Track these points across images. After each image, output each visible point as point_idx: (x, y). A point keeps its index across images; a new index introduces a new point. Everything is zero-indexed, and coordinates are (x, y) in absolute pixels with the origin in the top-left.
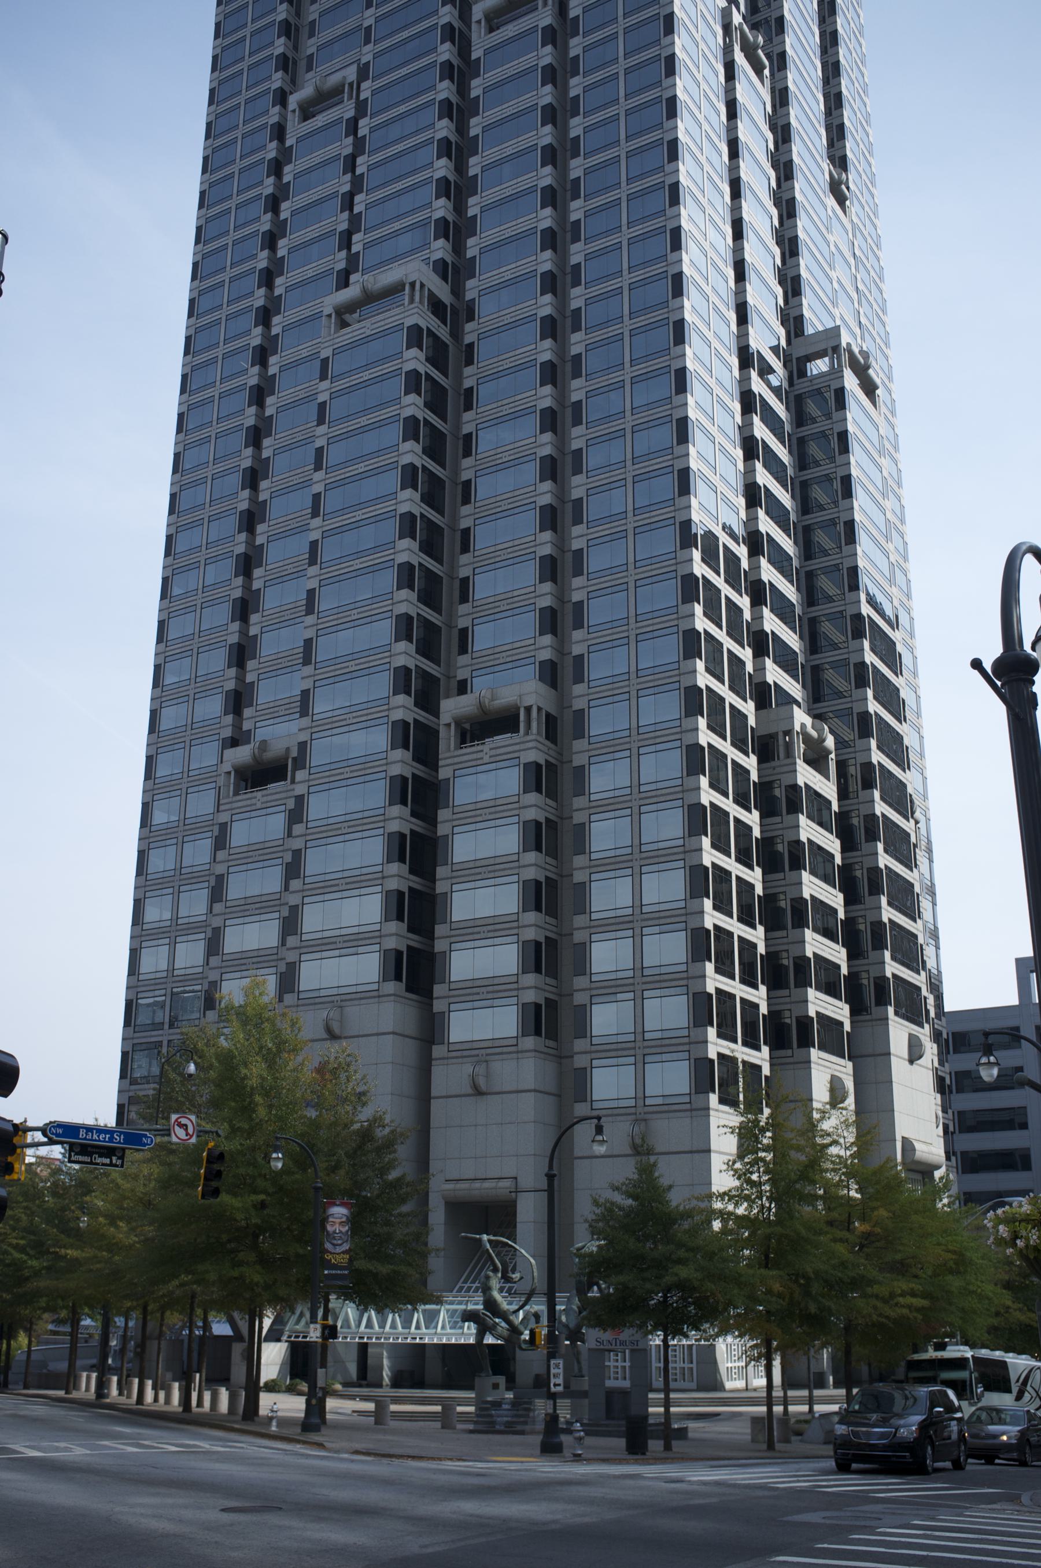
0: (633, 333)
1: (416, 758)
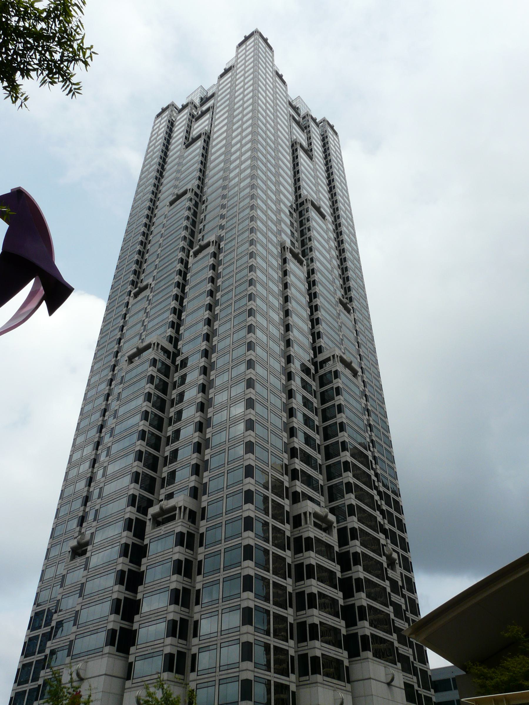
0: (222, 682)
1: (138, 511)
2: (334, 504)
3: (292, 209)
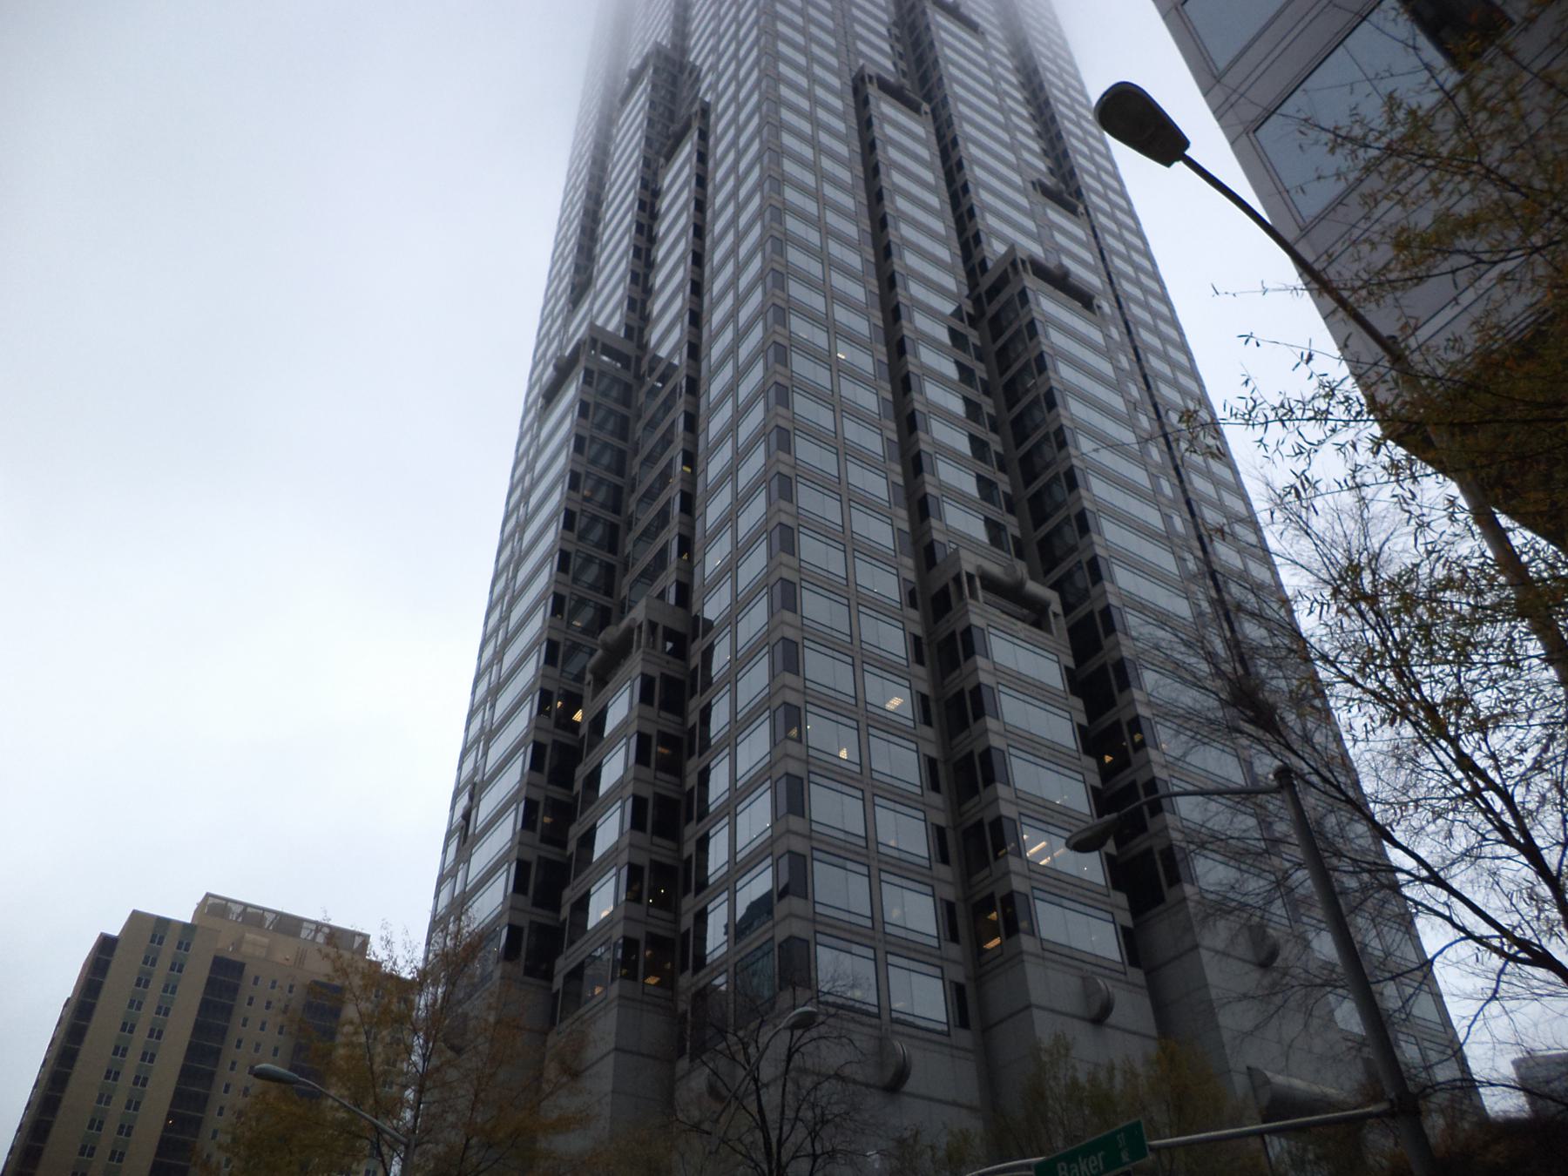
2: (1056, 574)
3: (962, 320)
